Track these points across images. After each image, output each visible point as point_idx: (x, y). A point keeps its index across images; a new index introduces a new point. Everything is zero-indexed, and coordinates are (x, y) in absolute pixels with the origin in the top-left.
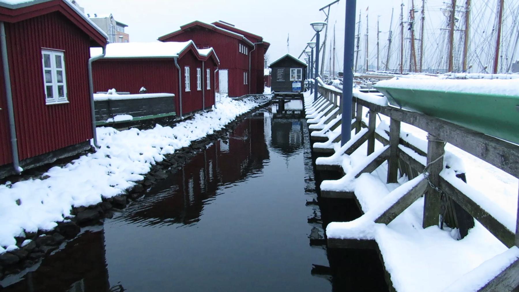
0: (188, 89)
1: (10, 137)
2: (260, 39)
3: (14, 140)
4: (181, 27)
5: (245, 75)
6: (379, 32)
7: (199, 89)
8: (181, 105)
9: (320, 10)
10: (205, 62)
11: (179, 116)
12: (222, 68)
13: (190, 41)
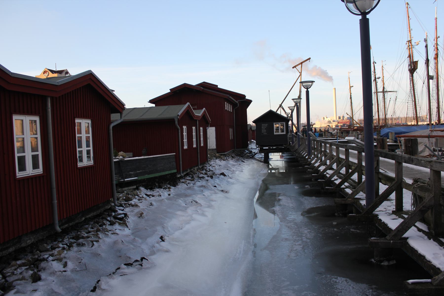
0: (186, 147)
1: (52, 199)
2: (244, 96)
3: (56, 202)
4: (170, 90)
5: (231, 130)
6: (351, 87)
7: (195, 146)
8: (181, 162)
9: (293, 68)
10: (199, 121)
11: (180, 173)
12: (211, 126)
13: (188, 103)
